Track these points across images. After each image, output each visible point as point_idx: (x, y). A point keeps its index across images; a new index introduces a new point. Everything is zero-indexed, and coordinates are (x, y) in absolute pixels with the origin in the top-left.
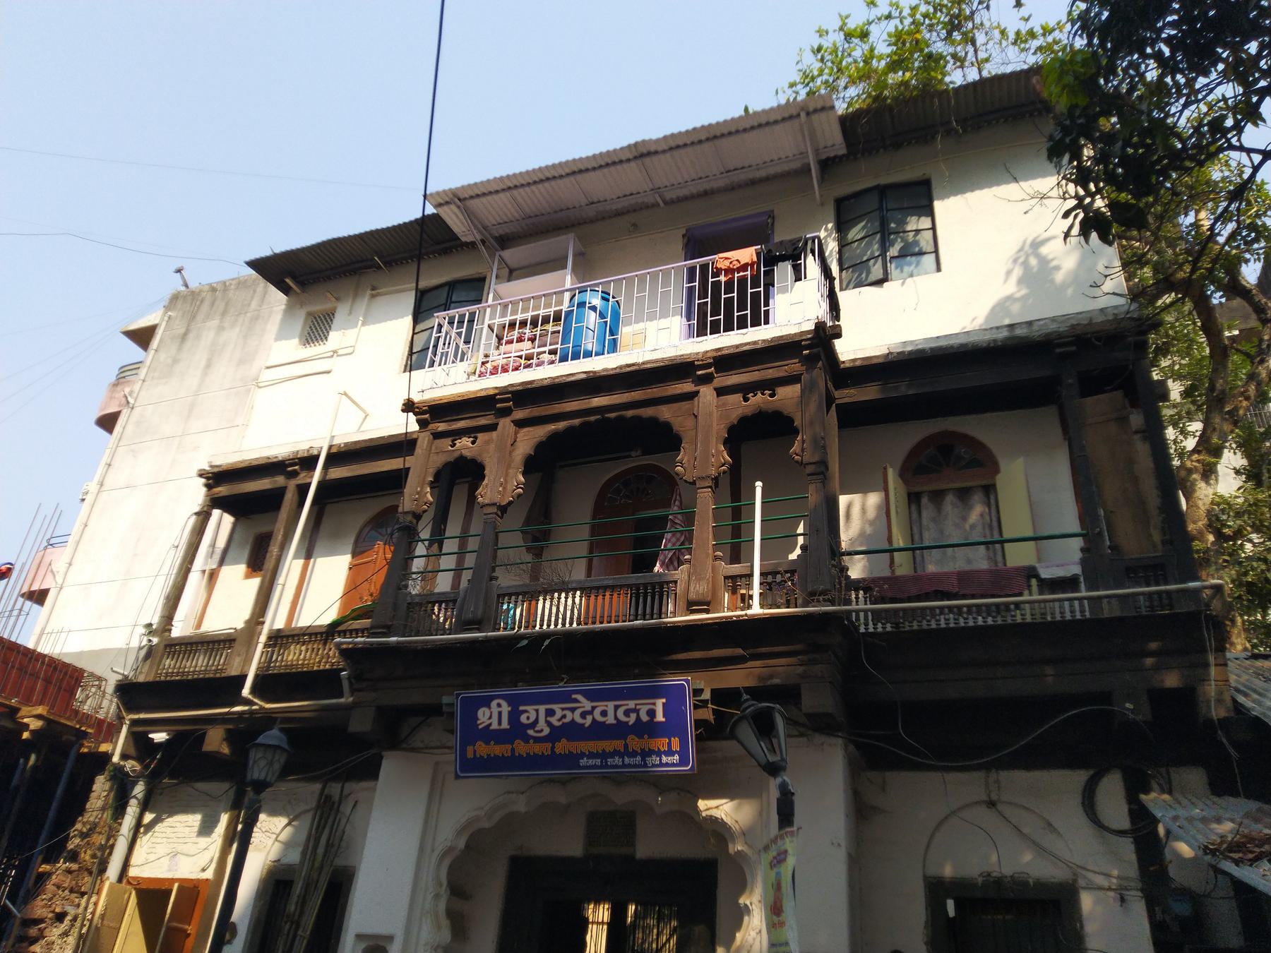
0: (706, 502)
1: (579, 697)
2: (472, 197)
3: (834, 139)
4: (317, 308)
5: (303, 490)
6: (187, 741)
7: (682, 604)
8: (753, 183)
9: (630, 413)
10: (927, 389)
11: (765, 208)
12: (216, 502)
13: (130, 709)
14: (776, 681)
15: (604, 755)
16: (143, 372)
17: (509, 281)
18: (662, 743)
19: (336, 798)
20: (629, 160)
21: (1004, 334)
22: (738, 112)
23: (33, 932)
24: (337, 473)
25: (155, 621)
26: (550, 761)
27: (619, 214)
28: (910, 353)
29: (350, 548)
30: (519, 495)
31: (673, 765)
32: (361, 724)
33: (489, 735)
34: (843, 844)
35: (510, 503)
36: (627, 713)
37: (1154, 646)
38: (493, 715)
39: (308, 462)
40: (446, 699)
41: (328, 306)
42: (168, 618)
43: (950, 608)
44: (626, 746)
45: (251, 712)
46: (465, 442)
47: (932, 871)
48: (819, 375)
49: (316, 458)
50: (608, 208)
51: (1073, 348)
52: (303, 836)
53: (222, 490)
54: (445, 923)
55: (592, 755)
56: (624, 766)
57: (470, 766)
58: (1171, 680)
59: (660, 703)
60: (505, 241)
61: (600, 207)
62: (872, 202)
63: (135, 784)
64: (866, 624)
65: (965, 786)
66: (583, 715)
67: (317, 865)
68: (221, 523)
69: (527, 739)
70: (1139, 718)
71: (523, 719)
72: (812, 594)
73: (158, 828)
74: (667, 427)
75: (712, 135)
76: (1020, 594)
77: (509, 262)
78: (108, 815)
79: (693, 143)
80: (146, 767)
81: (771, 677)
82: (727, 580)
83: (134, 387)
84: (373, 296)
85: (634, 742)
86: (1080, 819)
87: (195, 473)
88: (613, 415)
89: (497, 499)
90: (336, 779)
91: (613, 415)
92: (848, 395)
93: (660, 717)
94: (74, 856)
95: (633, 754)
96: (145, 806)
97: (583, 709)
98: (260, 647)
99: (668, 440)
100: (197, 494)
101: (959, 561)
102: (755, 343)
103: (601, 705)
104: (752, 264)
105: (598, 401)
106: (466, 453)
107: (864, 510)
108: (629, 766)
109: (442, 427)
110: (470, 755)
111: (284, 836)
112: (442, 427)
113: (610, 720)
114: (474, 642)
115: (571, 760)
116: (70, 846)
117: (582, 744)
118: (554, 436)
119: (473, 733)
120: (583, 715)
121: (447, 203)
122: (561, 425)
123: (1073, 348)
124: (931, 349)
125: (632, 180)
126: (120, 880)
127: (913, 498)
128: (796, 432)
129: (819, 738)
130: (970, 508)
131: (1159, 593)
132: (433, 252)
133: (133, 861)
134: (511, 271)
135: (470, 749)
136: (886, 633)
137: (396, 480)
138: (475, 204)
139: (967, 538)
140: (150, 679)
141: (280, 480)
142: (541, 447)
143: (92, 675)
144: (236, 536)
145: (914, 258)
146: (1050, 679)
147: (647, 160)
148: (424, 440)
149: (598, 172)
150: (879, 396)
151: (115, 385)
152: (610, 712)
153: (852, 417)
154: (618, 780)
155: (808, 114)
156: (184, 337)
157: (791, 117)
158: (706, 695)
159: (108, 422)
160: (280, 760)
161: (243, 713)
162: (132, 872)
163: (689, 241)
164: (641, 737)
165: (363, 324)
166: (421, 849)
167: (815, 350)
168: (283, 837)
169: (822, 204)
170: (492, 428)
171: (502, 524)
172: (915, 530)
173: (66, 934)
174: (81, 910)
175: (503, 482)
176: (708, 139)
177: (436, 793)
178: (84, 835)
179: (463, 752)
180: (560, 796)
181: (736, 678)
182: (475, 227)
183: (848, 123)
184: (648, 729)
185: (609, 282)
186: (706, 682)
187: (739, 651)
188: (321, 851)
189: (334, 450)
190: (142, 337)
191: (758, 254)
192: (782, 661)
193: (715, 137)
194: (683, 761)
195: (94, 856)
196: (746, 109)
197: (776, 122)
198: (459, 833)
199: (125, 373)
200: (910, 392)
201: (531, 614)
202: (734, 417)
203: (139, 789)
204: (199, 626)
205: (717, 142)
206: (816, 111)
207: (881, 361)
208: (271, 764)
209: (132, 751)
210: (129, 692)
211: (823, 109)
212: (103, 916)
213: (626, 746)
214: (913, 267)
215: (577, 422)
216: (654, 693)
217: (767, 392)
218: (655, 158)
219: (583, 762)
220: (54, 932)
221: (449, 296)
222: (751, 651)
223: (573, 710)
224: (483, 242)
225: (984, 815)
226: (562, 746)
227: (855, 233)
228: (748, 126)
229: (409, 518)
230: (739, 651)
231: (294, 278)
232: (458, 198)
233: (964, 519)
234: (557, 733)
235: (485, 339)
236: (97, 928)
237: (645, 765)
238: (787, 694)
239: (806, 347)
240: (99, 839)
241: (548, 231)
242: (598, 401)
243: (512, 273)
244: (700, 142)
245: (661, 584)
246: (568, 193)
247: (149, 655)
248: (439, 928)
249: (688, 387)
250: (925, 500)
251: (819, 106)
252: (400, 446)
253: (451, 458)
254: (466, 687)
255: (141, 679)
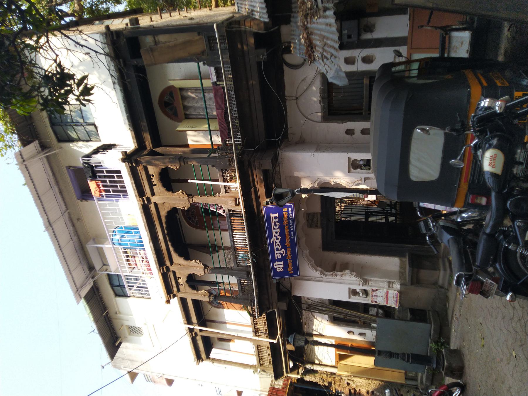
0: (198, 199)
1: (271, 241)
2: (76, 286)
3: (33, 147)
4: (126, 332)
5: (201, 331)
6: (292, 355)
7: (237, 207)
8: (54, 174)
9: (164, 225)
10: (144, 115)
11: (65, 169)
12: (208, 356)
13: (283, 375)
14: (262, 177)
15: (290, 231)
16: (148, 373)
17: (109, 265)
18: (285, 214)
19: (307, 305)
20: (53, 229)
21: (117, 86)
22: (26, 188)
23: (353, 391)
24: (194, 319)
25: (252, 370)
26: (291, 245)
27: (73, 225)
28: (129, 122)
29: (221, 310)
30: (200, 261)
31: (292, 210)
32: (284, 306)
33: (285, 267)
34: (313, 154)
35: (203, 264)
36: (276, 225)
37: (239, 46)
38: (279, 267)
39: (191, 330)
40: (275, 281)
41: (125, 328)
42: (251, 366)
43: (231, 113)
44: (287, 225)
45: (281, 337)
46: (180, 281)
47: (320, 119)
48: (144, 159)
49: (190, 329)
50: (72, 232)
51: (121, 60)
52: (320, 315)
53: (203, 356)
54: (343, 272)
55: (290, 235)
56: (293, 225)
57: (296, 272)
58: (252, 41)
59: (272, 215)
60: (91, 268)
61: (73, 234)
62: (58, 129)
63: (306, 368)
64: (238, 141)
65: (291, 106)
66: (277, 239)
67: (328, 310)
68: (215, 353)
69: (286, 256)
70: (265, 54)
71: (280, 257)
72: (230, 164)
73: (320, 358)
74: (169, 212)
75: (38, 198)
76: (223, 88)
77: (100, 267)
78: (317, 375)
79: (42, 205)
80: (301, 366)
81: (260, 179)
82: (228, 194)
83: (154, 376)
84: (120, 313)
85: (285, 222)
86: (301, 70)
87: (198, 366)
88: (166, 231)
89: (202, 269)
90: (300, 307)
91: (166, 231)
92: (149, 144)
93: (277, 215)
94: (330, 383)
95: (289, 222)
96: (313, 363)
97: (275, 239)
98: (260, 339)
99: (173, 212)
100: (206, 364)
101: (212, 104)
102: (132, 183)
103: (274, 234)
104: (97, 183)
105: (161, 237)
106: (185, 280)
107: (194, 136)
108: (293, 223)
109: (175, 289)
110: (292, 272)
111: (320, 319)
112: (175, 289)
113: (278, 230)
114: (255, 275)
115: (292, 241)
116: (327, 385)
117: (287, 238)
118: (176, 251)
119: (285, 272)
120: (277, 239)
121: (79, 295)
122: (171, 249)
123: (121, 60)
124: (127, 114)
125: (61, 226)
126: (337, 367)
127: (187, 117)
128: (167, 168)
129: (280, 160)
130: (189, 96)
131: (219, 39)
132: (98, 293)
133: (330, 364)
134: (104, 265)
135: (290, 273)
136: (241, 135)
137: (197, 303)
138: (78, 286)
139: (201, 98)
140: (272, 370)
141: (199, 338)
142: (180, 255)
143: (271, 384)
144: (219, 347)
145: (83, 113)
146: (254, 82)
147: (51, 221)
148: (180, 295)
149: (59, 239)
150: (148, 133)
151: (155, 382)
152: (276, 231)
153: (157, 142)
154: (297, 222)
155: (24, 161)
156: (132, 361)
157: (26, 167)
158: (268, 200)
159: (170, 382)
160: (298, 337)
161: (282, 340)
162: (334, 364)
163: (83, 199)
164: (284, 221)
165: (132, 315)
166: (322, 281)
167: (133, 161)
168: (320, 320)
169: (61, 148)
170: (174, 273)
171: (211, 266)
172: (199, 117)
173: (353, 381)
174: (346, 378)
175: (195, 267)
176: (40, 199)
177: (306, 278)
178: (323, 381)
179: (291, 274)
180: (303, 240)
181: (262, 190)
182: (87, 281)
183: (25, 143)
184: (281, 218)
185: (106, 226)
186: (264, 201)
187: (252, 190)
188: (324, 309)
189: (186, 322)
190: (133, 376)
191: (92, 180)
192: (255, 175)
193: (38, 196)
194: (291, 207)
195: (330, 377)
196: (24, 185)
197: (29, 173)
198: (316, 270)
199: (149, 379)
200: (145, 121)
201: (242, 249)
202: (163, 189)
203: (308, 366)
204: (253, 355)
205: (40, 195)
206: (22, 158)
207: (133, 133)
208: (299, 340)
209: (296, 371)
210: (278, 375)
211: (21, 155)
212: (348, 372)
213: (287, 225)
214: (88, 114)
215: (169, 244)
216: (269, 218)
217: (152, 177)
218: (50, 219)
219: (292, 238)
220: (353, 385)
221: (117, 286)
222: (252, 186)
223: (276, 242)
224: (93, 278)
225: (302, 101)
226: (288, 245)
227: (73, 135)
228: (32, 184)
229: (211, 297)
230: (252, 190)
231: (115, 342)
232: (77, 291)
233: (194, 98)
234: (284, 246)
235: (136, 273)
236: (351, 373)
237: (293, 218)
238: (266, 173)
239: (132, 164)
240: (325, 376)
241: (84, 252)
242: (161, 237)
243: (105, 264)
244: (41, 202)
245: (230, 214)
246: (69, 249)
247: (264, 371)
248: (345, 274)
249: (152, 206)
250: (188, 113)
251: (20, 157)
252: (183, 302)
253: (187, 285)
254: (270, 275)
255: (273, 372)
